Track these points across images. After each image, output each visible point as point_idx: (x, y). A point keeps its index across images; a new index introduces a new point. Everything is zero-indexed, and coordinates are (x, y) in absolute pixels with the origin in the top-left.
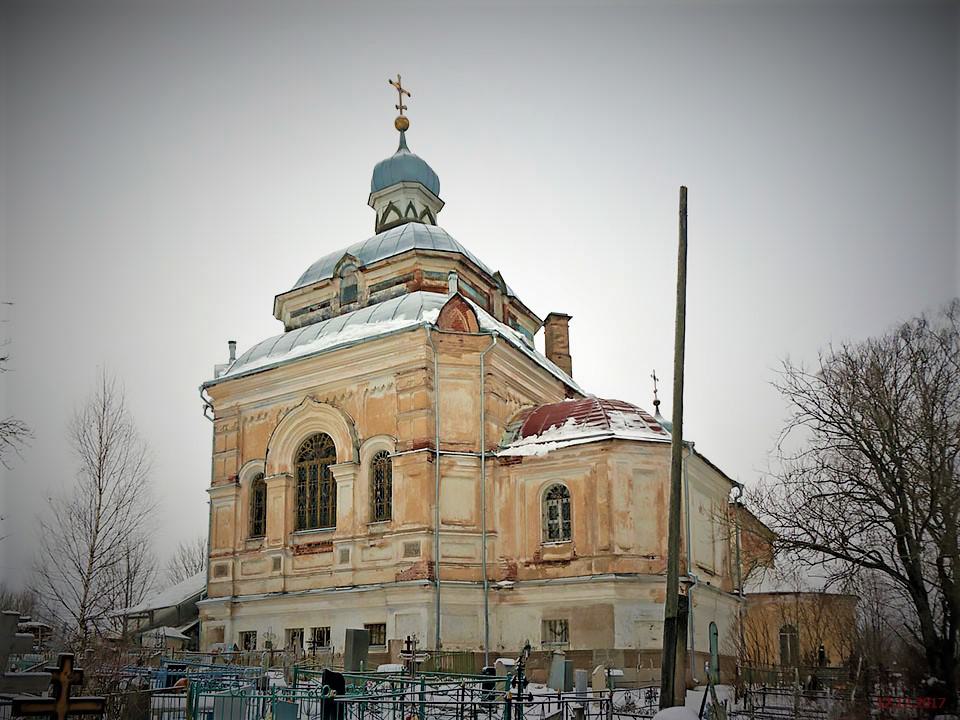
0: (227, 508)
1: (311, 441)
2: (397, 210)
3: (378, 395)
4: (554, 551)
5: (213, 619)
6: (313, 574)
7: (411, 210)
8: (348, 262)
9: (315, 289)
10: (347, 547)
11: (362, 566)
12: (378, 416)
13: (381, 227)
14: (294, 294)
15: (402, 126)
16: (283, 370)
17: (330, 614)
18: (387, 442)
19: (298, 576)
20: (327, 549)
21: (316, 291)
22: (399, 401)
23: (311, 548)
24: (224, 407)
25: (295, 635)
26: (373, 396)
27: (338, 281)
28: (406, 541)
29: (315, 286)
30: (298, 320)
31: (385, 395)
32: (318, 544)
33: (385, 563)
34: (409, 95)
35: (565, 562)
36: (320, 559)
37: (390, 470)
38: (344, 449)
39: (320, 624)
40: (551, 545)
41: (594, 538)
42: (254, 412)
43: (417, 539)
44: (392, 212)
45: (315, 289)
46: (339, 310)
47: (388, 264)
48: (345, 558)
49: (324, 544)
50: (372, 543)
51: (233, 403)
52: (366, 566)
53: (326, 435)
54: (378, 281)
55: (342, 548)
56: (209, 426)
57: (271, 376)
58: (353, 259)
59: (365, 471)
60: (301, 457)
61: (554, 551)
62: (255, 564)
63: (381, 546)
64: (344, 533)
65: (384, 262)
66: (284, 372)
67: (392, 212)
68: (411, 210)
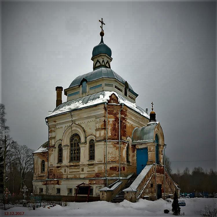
1: (72, 138)
13: (95, 68)
14: (69, 89)
15: (102, 34)
34: (105, 25)
37: (94, 145)
38: (83, 140)
44: (98, 62)
53: (76, 134)
55: (82, 168)
56: (92, 56)
59: (88, 145)
60: (72, 139)
67: (98, 62)
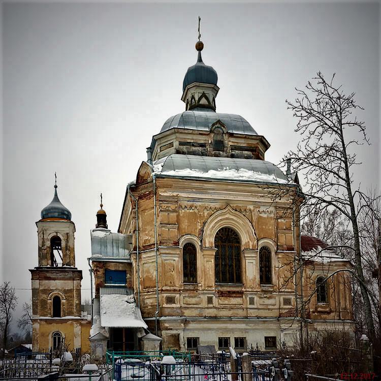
0: (172, 261)
2: (207, 99)
3: (263, 215)
4: (322, 307)
5: (171, 329)
6: (232, 308)
7: (193, 100)
8: (218, 125)
9: (200, 134)
10: (253, 296)
11: (260, 307)
12: (264, 227)
15: (200, 47)
16: (214, 184)
17: (246, 331)
18: (271, 243)
19: (222, 308)
20: (239, 295)
21: (200, 136)
22: (278, 223)
23: (230, 294)
24: (165, 194)
25: (224, 343)
26: (260, 215)
27: (212, 135)
28: (284, 297)
29: (201, 132)
30: (184, 148)
31: (268, 217)
32: (234, 292)
33: (273, 307)
35: (328, 313)
36: (234, 301)
39: (239, 335)
40: (321, 304)
41: (339, 303)
42: (186, 203)
43: (291, 297)
45: (200, 134)
46: (213, 153)
47: (245, 138)
48: (252, 302)
49: (238, 292)
50: (265, 296)
51: (175, 194)
52: (262, 307)
54: (236, 144)
57: (205, 185)
58: (223, 125)
61: (322, 307)
62: (191, 299)
63: (269, 298)
64: (252, 288)
65: (244, 136)
66: (214, 186)
68: (193, 100)
